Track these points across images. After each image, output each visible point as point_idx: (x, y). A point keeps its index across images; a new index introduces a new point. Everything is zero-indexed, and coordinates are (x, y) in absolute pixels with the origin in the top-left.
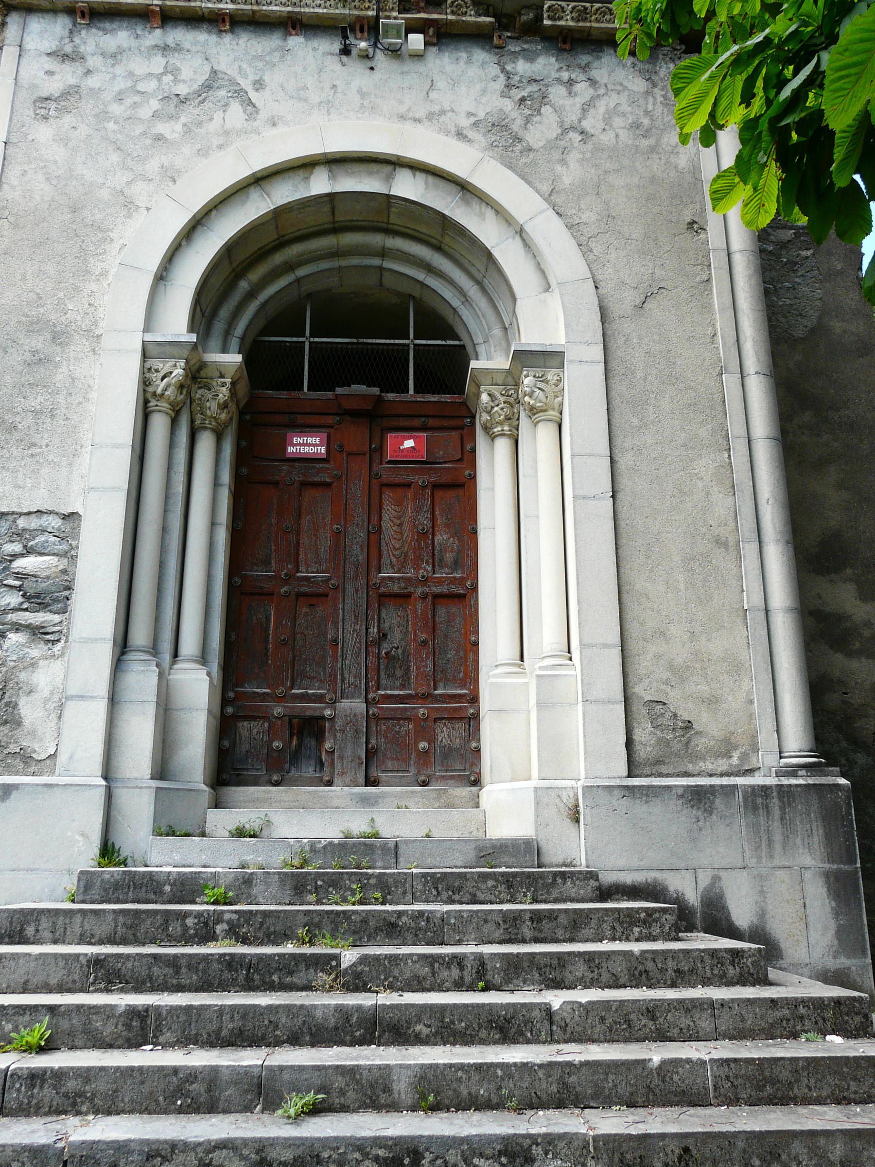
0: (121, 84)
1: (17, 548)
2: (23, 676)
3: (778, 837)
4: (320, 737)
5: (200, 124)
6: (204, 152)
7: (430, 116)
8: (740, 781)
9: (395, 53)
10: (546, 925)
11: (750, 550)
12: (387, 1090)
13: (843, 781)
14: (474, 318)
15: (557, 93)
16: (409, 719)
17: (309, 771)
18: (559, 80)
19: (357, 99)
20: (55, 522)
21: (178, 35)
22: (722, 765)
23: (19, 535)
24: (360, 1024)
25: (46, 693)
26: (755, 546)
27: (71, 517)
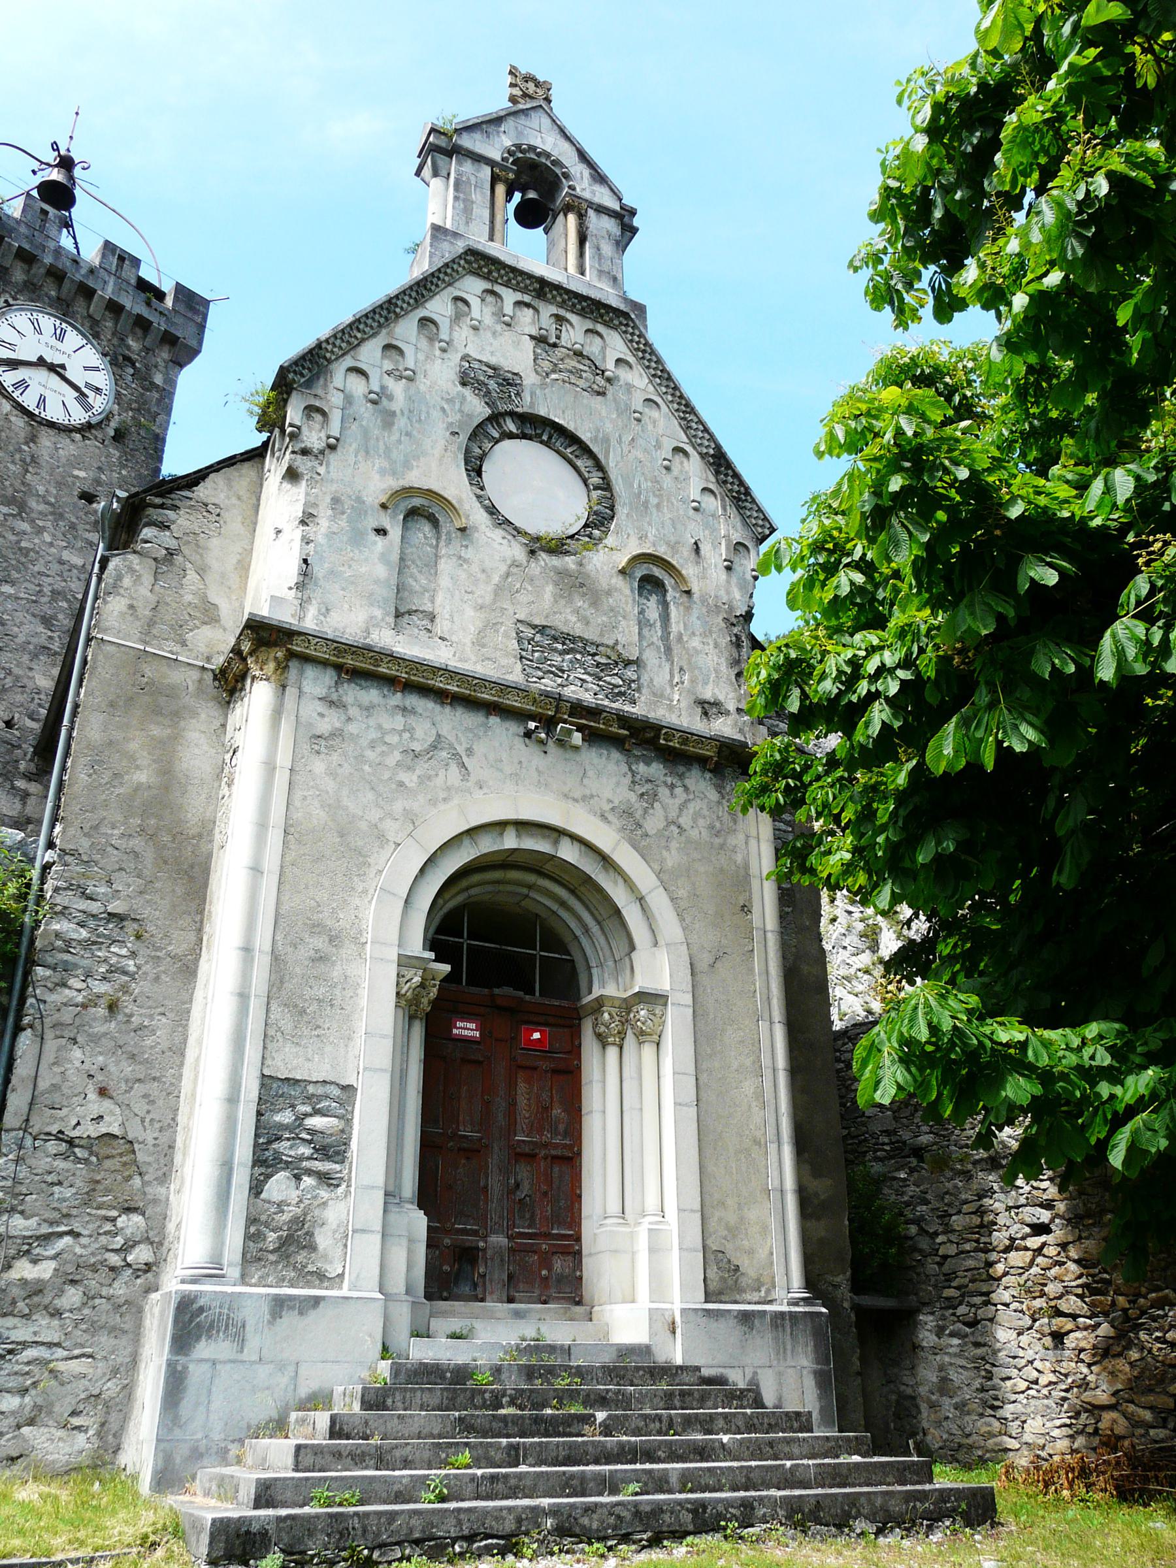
0: (373, 734)
1: (308, 1109)
2: (316, 1212)
3: (789, 1347)
4: (473, 1262)
5: (429, 778)
6: (433, 802)
7: (585, 798)
8: (767, 1308)
9: (561, 743)
10: (688, 1399)
11: (772, 1148)
12: (667, 1482)
13: (824, 1310)
14: (594, 945)
15: (663, 792)
16: (535, 1252)
17: (466, 1289)
18: (665, 783)
19: (535, 774)
20: (336, 1092)
21: (413, 700)
22: (755, 1296)
23: (309, 1098)
24: (630, 1452)
25: (334, 1226)
26: (775, 1146)
27: (349, 1089)
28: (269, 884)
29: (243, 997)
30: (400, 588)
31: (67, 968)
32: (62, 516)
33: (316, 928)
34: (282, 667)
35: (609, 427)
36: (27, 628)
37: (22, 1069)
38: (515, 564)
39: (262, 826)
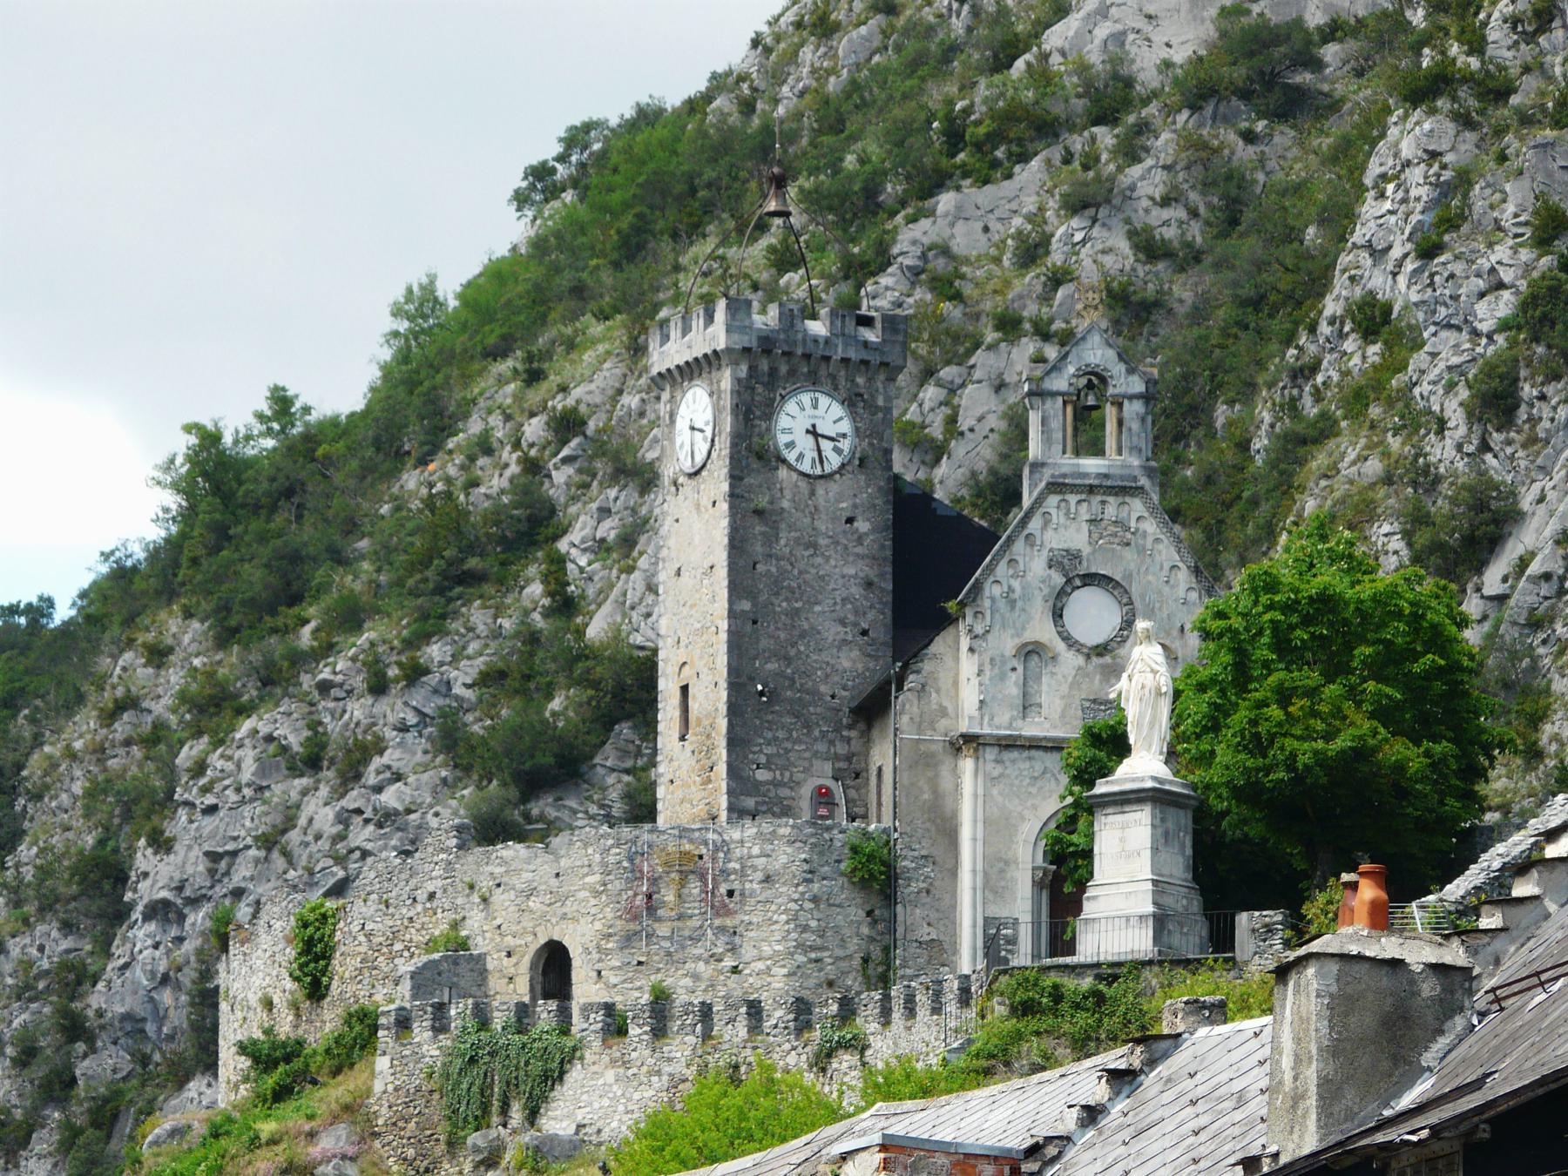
6: (1044, 799)
21: (1033, 753)
28: (980, 844)
29: (974, 889)
30: (1025, 695)
31: (909, 879)
32: (838, 543)
33: (1000, 859)
34: (976, 750)
35: (1132, 566)
36: (833, 631)
37: (900, 918)
38: (1080, 668)
39: (975, 821)
